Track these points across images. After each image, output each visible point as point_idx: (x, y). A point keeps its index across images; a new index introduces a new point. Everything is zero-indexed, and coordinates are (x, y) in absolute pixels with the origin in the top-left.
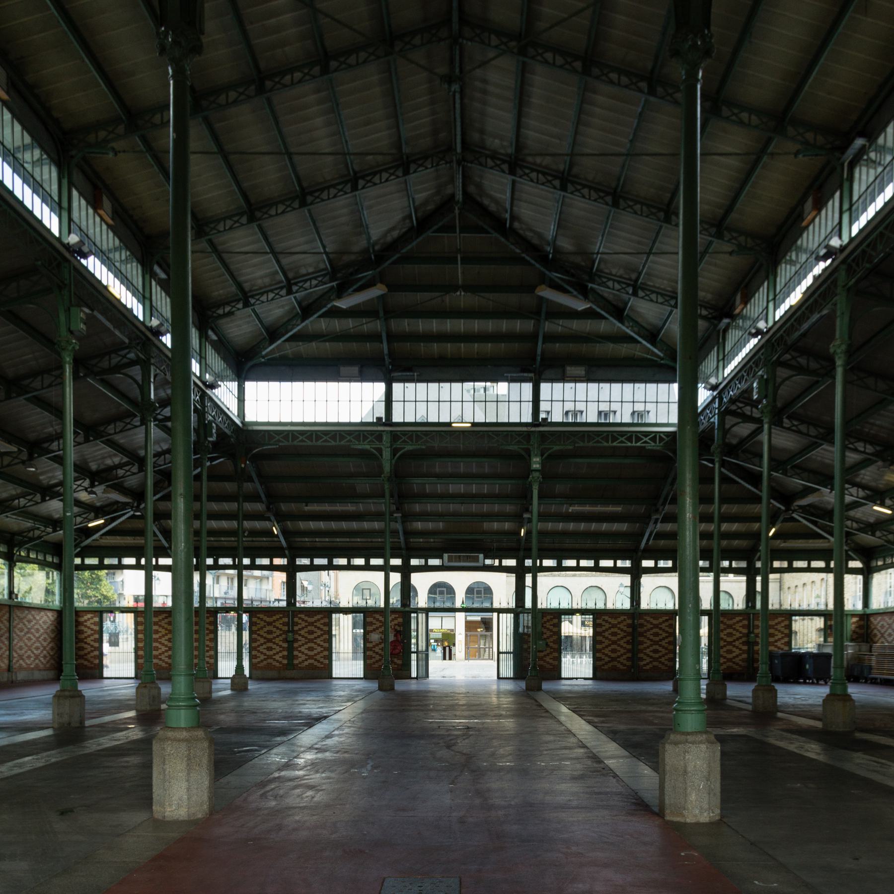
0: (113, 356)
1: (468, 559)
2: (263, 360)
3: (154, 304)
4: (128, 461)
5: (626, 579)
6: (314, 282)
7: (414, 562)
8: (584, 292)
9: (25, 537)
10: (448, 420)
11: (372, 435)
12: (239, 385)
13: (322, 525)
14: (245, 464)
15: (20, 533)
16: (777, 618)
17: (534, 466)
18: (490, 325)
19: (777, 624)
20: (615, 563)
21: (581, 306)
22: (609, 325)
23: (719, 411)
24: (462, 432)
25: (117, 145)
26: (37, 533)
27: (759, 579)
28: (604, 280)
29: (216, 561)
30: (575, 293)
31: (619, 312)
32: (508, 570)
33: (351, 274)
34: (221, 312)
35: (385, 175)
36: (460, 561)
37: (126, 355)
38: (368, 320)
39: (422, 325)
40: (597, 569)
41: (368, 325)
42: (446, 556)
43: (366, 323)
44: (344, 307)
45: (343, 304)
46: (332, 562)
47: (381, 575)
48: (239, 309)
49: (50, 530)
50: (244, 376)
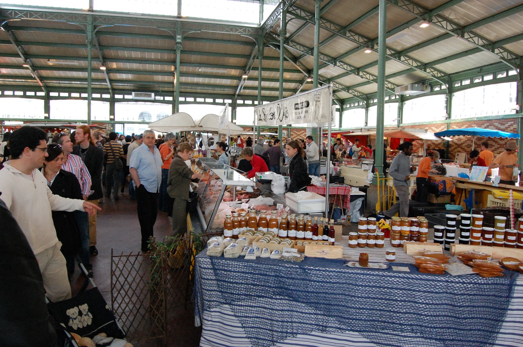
1: (146, 95)
5: (108, 104)
7: (117, 96)
11: (21, 13)
13: (207, 80)
16: (301, 131)
17: (178, 40)
19: (301, 134)
20: (164, 98)
23: (283, 10)
32: (168, 102)
40: (214, 103)
46: (71, 95)
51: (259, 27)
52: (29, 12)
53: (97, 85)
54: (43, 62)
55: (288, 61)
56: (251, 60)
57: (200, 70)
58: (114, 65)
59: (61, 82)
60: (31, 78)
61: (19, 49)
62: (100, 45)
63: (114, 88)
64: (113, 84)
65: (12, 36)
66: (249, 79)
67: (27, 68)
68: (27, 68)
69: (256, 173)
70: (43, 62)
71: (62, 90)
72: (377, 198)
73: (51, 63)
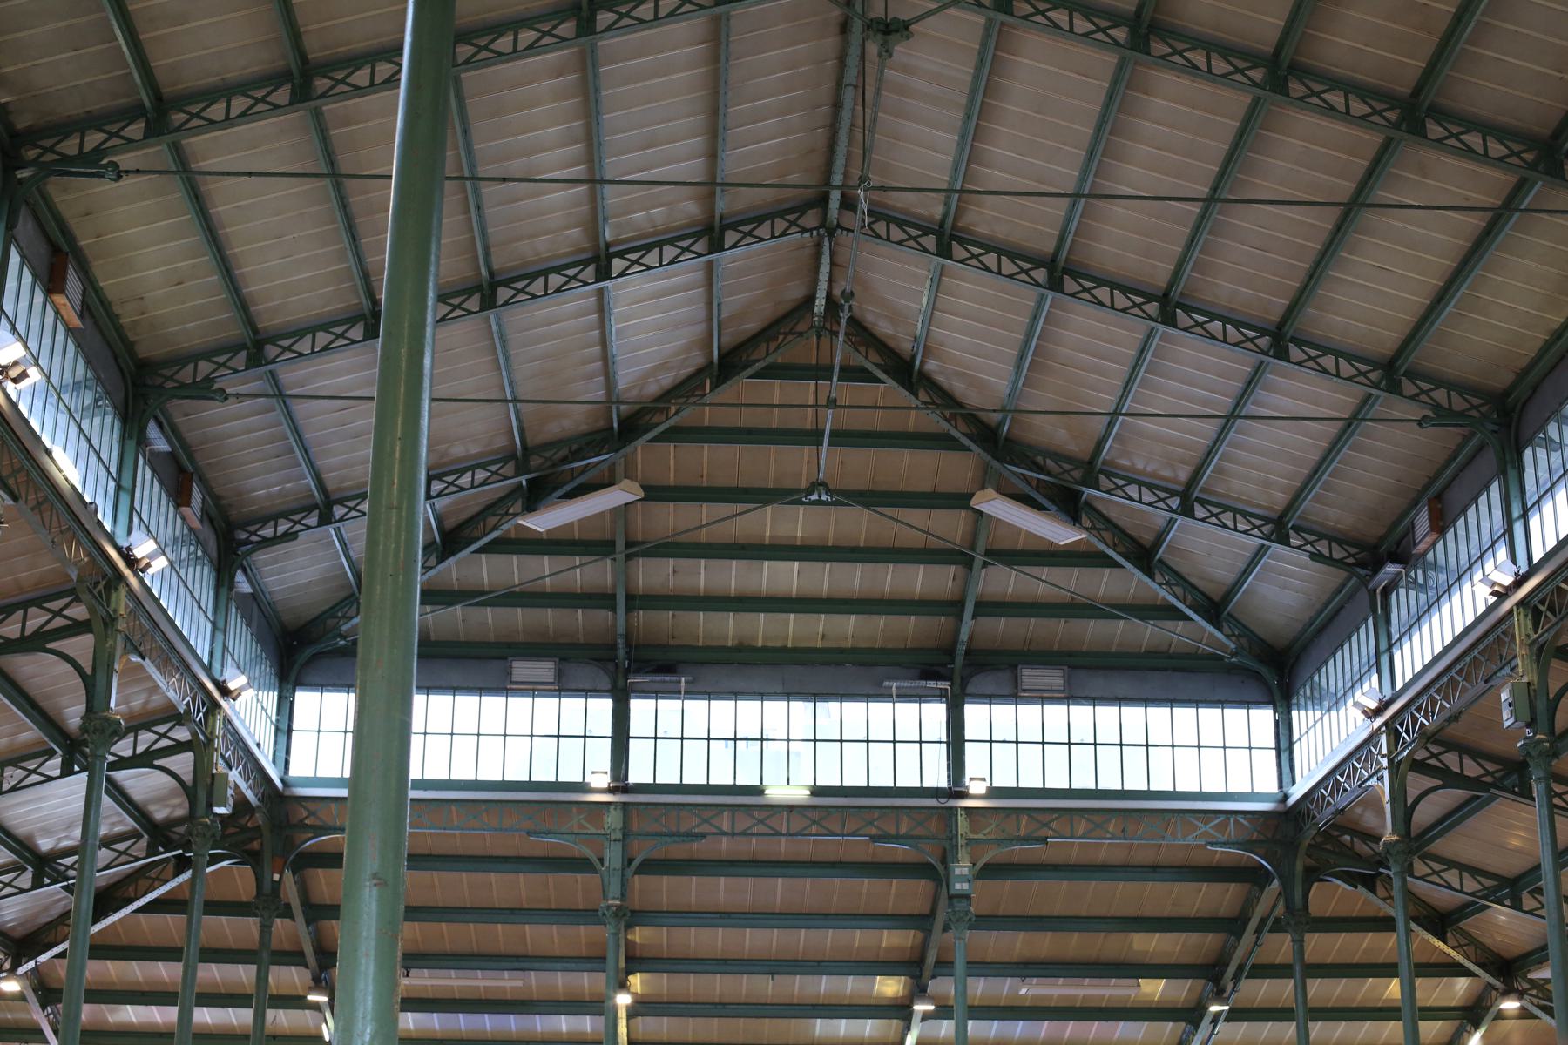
0: (32, 610)
2: (342, 642)
3: (137, 505)
4: (14, 863)
6: (481, 475)
8: (1069, 505)
10: (754, 781)
12: (280, 698)
14: (281, 875)
17: (958, 886)
18: (855, 578)
21: (1062, 534)
22: (1128, 582)
23: (1391, 761)
25: (126, 160)
28: (1121, 482)
30: (1053, 508)
31: (1144, 555)
33: (564, 460)
34: (268, 532)
35: (670, 252)
37: (62, 610)
38: (586, 559)
39: (704, 576)
41: (584, 573)
43: (581, 565)
44: (541, 530)
45: (541, 522)
48: (309, 528)
50: (293, 678)
51: (1281, 808)
55: (1118, 565)
56: (1248, 937)
57: (1023, 991)
66: (1235, 1015)
72: (780, 142)
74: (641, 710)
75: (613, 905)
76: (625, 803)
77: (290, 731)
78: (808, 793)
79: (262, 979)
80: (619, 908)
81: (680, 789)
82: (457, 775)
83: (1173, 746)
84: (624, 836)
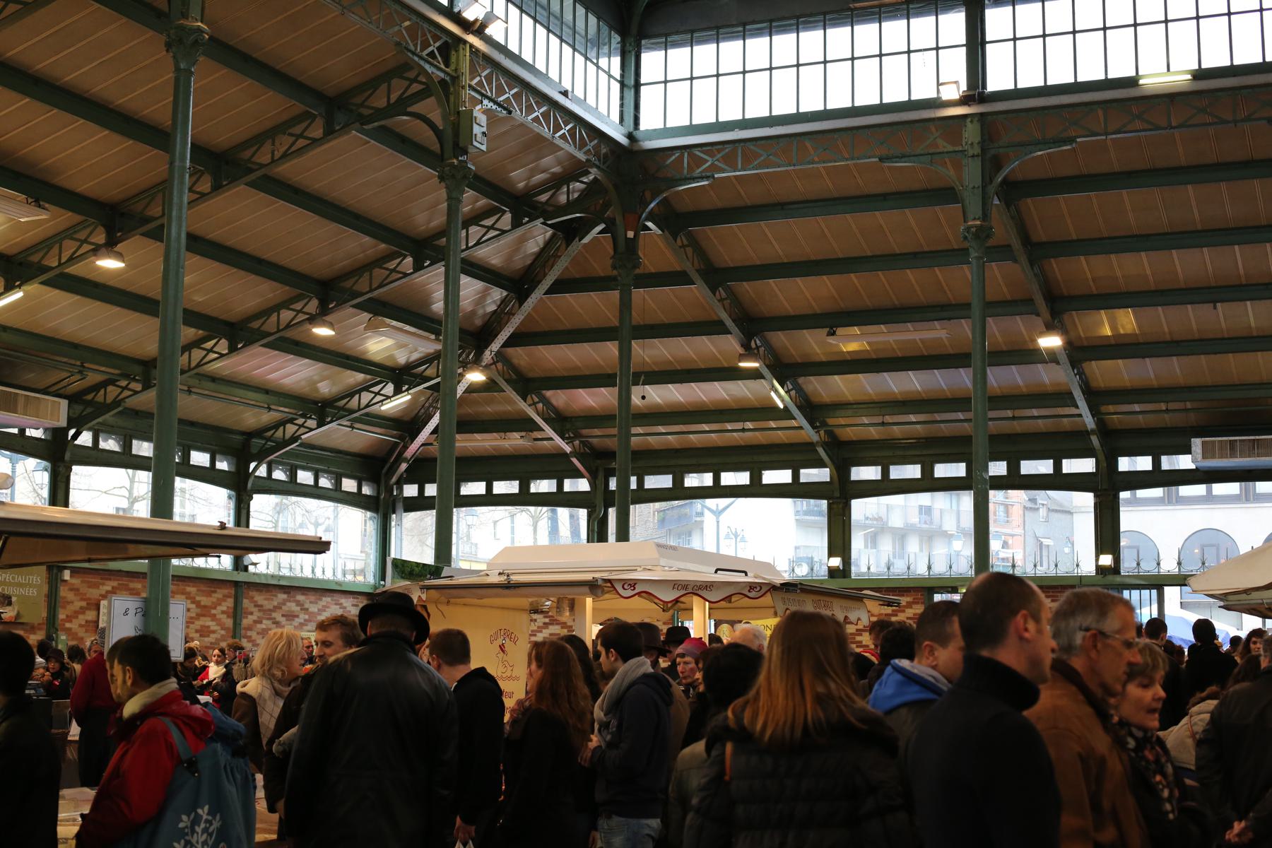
5: (1085, 501)
9: (269, 439)
10: (1131, 73)
15: (259, 433)
24: (1170, 99)
26: (291, 429)
27: (612, 513)
29: (1014, 468)
32: (573, 500)
36: (1233, 455)
42: (1197, 443)
46: (528, 487)
47: (966, 500)
49: (311, 423)
52: (740, 146)
53: (1037, 419)
54: (814, 343)
58: (1107, 324)
59: (938, 417)
60: (766, 411)
61: (721, 300)
62: (1027, 241)
63: (592, 448)
64: (1104, 409)
65: (689, 250)
67: (755, 375)
68: (755, 375)
69: (90, 793)
70: (814, 343)
71: (693, 461)
73: (852, 342)
74: (651, 61)
75: (972, 226)
76: (982, 114)
77: (637, 85)
78: (1189, 77)
79: (625, 353)
80: (979, 228)
81: (1077, 87)
82: (805, 108)
83: (1229, 14)
84: (983, 150)
